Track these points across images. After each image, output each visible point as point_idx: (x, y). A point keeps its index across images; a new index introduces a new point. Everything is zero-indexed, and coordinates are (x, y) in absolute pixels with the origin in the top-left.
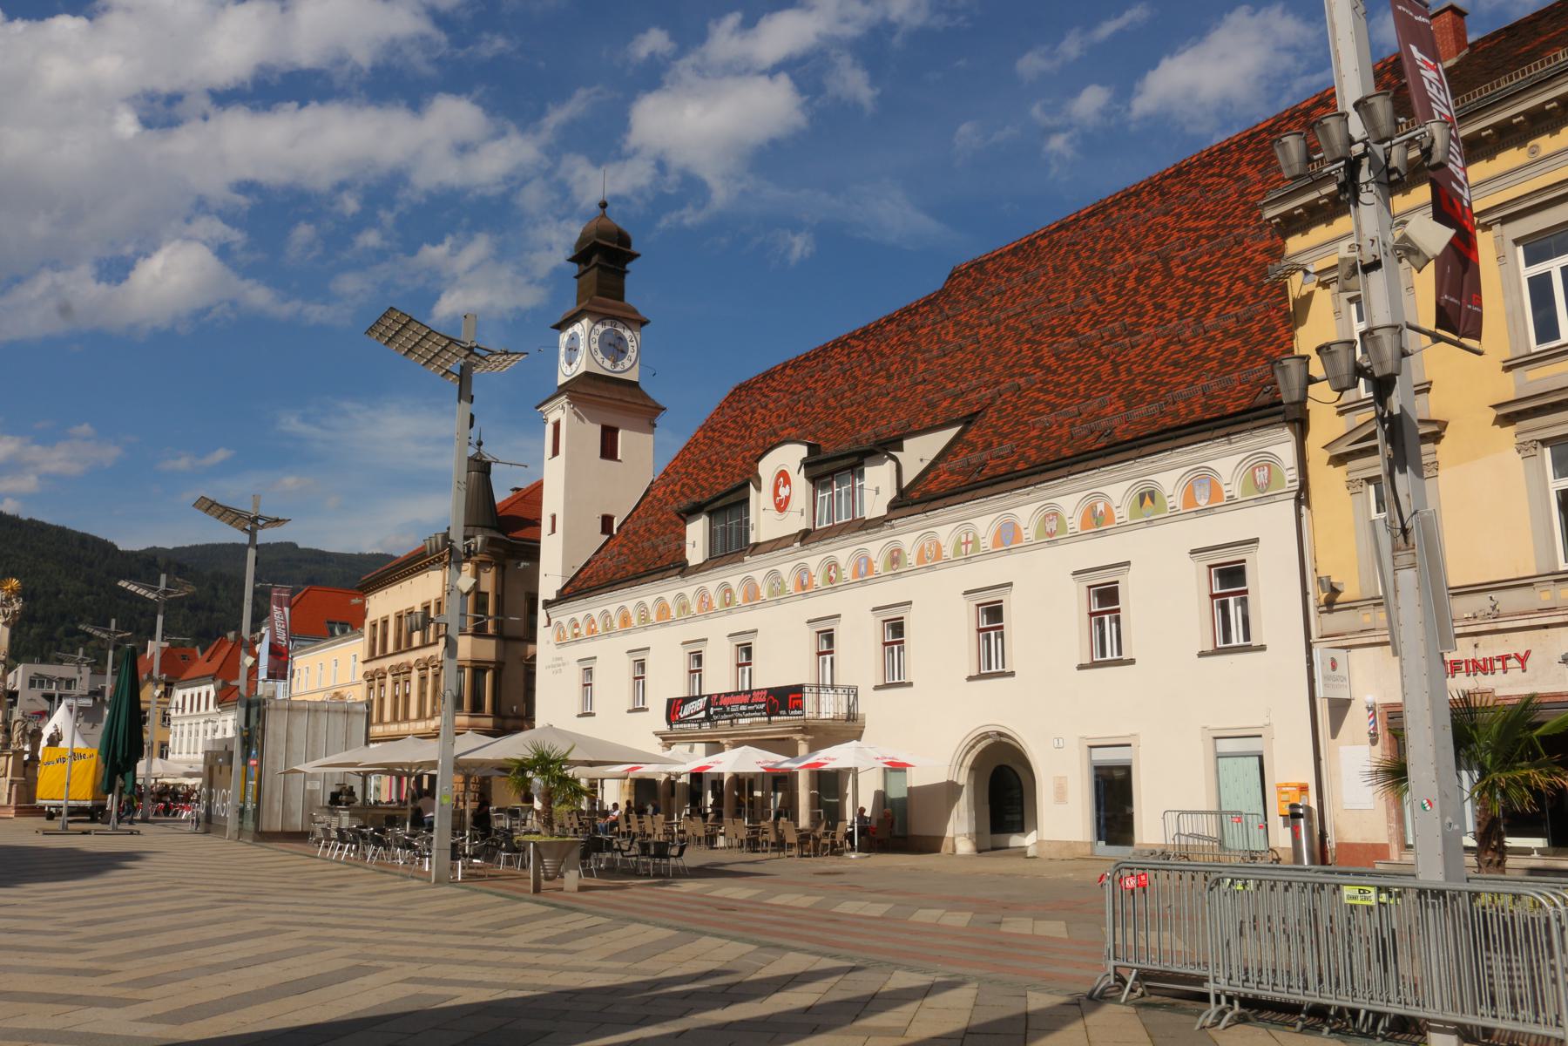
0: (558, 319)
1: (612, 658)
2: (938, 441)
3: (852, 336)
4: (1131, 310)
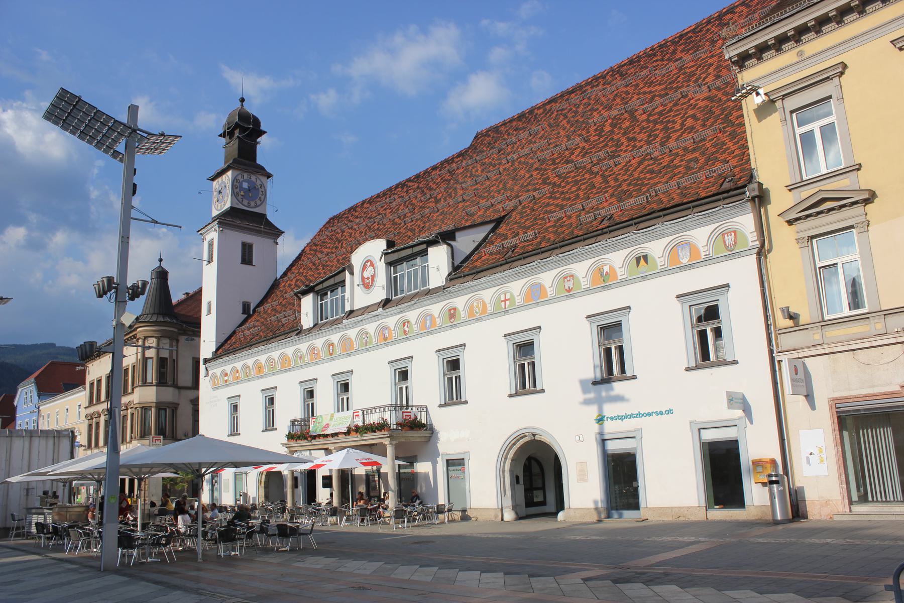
0: (212, 173)
1: (251, 397)
3: (409, 180)
4: (610, 144)
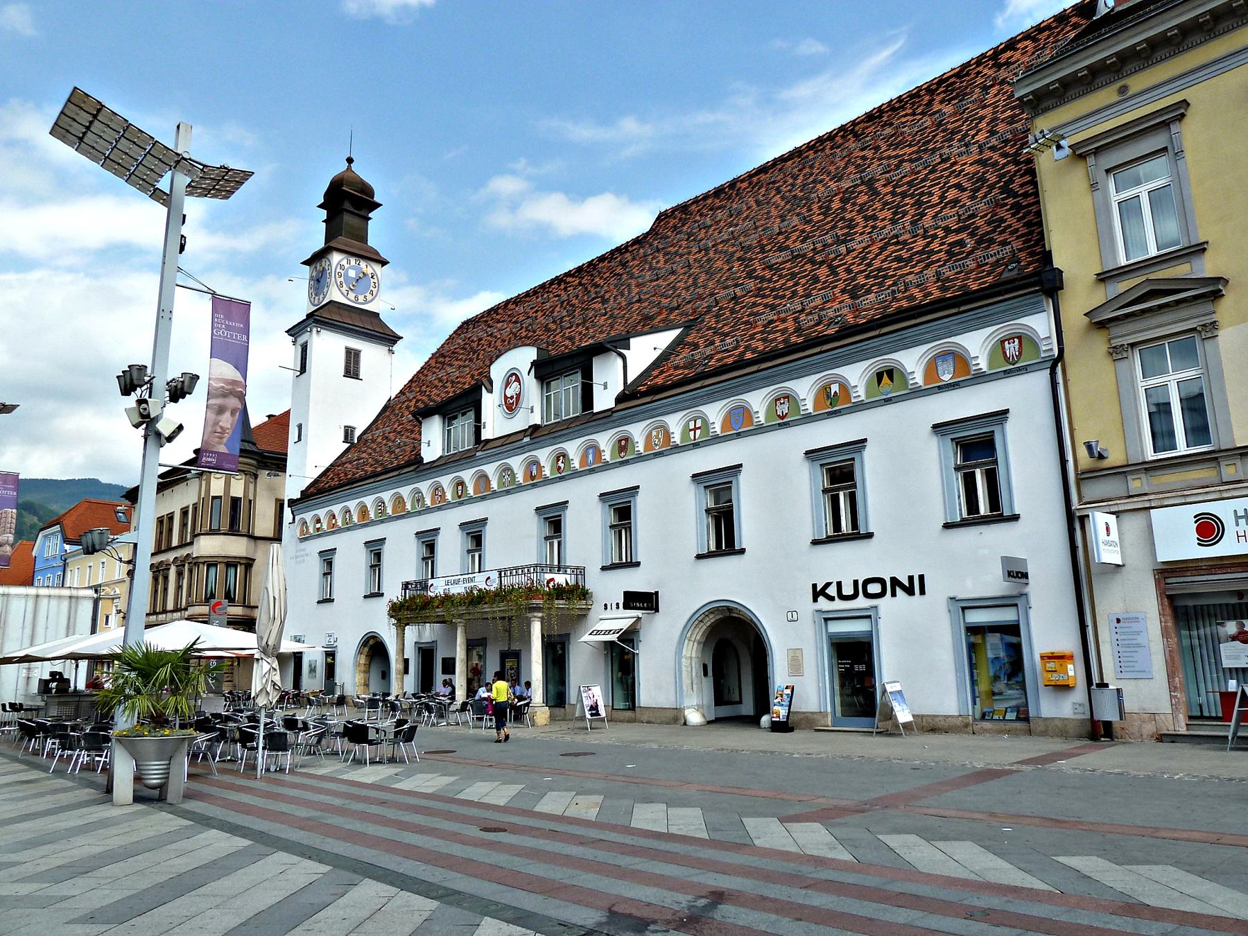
2: (665, 339)
3: (568, 274)
